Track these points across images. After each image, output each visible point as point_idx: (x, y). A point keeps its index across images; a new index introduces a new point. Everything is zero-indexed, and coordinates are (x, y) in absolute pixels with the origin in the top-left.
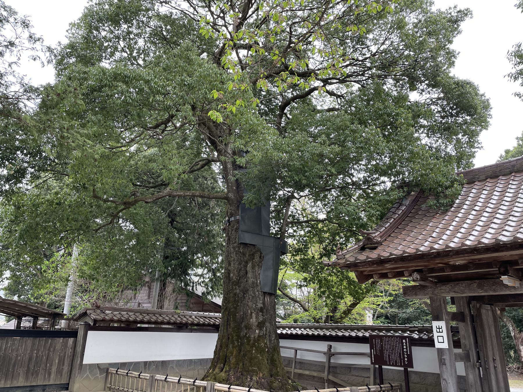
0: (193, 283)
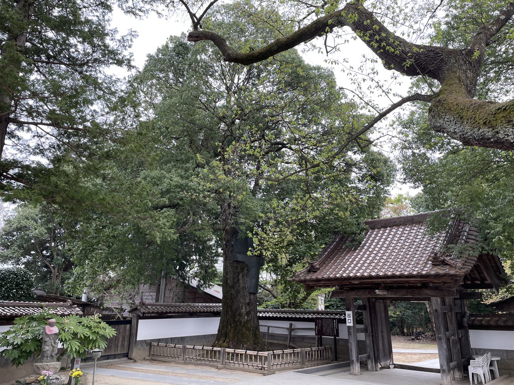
0: (189, 278)
